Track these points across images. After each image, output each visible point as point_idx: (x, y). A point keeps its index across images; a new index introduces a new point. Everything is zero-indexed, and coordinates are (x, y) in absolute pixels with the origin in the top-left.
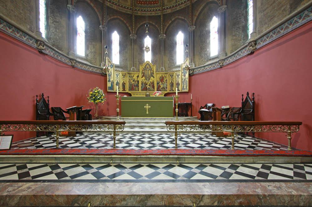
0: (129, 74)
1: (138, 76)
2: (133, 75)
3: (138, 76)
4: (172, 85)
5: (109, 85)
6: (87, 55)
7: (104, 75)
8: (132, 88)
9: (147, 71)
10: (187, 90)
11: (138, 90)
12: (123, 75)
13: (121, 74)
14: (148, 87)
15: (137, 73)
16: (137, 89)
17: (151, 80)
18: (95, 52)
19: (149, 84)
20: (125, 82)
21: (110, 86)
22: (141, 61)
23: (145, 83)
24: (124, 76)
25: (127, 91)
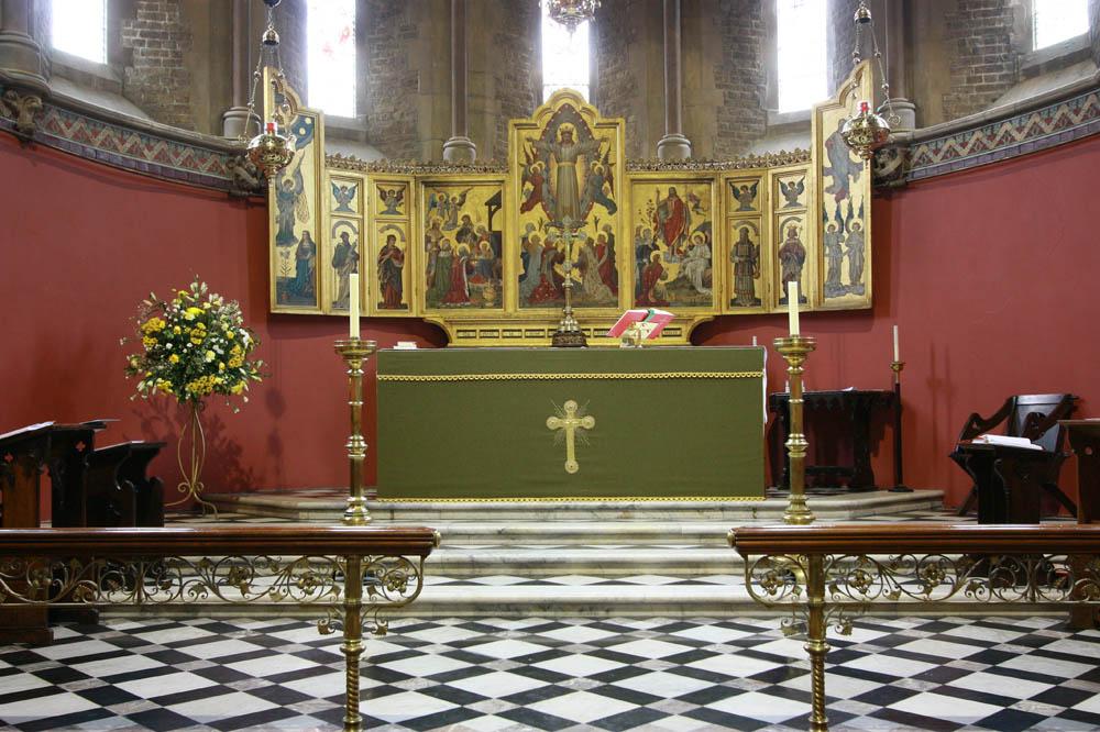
0: (428, 184)
1: (495, 203)
2: (455, 193)
3: (495, 203)
4: (747, 258)
5: (283, 263)
6: (121, 56)
7: (246, 192)
8: (450, 285)
9: (564, 170)
10: (860, 298)
11: (499, 303)
12: (383, 195)
13: (370, 190)
14: (570, 275)
15: (491, 177)
16: (489, 295)
17: (589, 231)
18: (182, 35)
19: (575, 258)
20: (400, 245)
21: (293, 274)
22: (516, 93)
23: (549, 247)
24: (393, 198)
25: (416, 308)
